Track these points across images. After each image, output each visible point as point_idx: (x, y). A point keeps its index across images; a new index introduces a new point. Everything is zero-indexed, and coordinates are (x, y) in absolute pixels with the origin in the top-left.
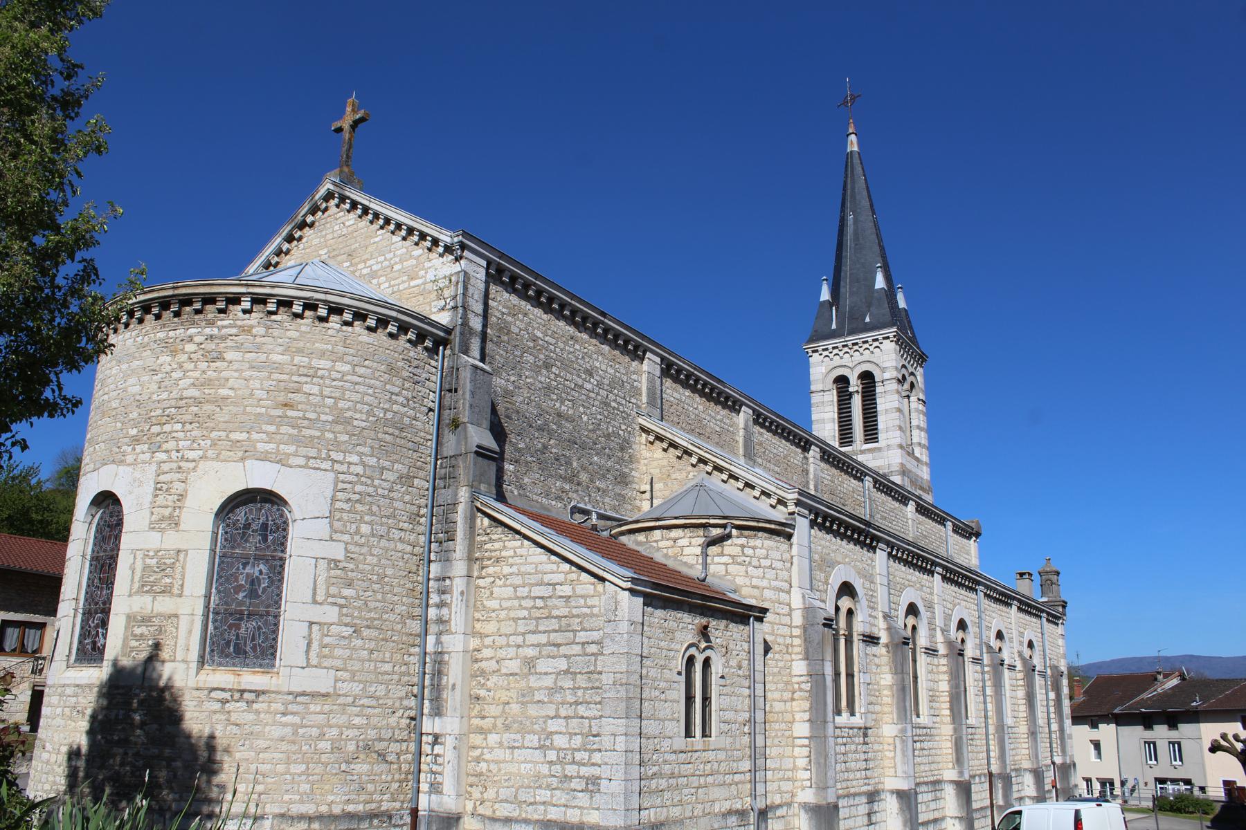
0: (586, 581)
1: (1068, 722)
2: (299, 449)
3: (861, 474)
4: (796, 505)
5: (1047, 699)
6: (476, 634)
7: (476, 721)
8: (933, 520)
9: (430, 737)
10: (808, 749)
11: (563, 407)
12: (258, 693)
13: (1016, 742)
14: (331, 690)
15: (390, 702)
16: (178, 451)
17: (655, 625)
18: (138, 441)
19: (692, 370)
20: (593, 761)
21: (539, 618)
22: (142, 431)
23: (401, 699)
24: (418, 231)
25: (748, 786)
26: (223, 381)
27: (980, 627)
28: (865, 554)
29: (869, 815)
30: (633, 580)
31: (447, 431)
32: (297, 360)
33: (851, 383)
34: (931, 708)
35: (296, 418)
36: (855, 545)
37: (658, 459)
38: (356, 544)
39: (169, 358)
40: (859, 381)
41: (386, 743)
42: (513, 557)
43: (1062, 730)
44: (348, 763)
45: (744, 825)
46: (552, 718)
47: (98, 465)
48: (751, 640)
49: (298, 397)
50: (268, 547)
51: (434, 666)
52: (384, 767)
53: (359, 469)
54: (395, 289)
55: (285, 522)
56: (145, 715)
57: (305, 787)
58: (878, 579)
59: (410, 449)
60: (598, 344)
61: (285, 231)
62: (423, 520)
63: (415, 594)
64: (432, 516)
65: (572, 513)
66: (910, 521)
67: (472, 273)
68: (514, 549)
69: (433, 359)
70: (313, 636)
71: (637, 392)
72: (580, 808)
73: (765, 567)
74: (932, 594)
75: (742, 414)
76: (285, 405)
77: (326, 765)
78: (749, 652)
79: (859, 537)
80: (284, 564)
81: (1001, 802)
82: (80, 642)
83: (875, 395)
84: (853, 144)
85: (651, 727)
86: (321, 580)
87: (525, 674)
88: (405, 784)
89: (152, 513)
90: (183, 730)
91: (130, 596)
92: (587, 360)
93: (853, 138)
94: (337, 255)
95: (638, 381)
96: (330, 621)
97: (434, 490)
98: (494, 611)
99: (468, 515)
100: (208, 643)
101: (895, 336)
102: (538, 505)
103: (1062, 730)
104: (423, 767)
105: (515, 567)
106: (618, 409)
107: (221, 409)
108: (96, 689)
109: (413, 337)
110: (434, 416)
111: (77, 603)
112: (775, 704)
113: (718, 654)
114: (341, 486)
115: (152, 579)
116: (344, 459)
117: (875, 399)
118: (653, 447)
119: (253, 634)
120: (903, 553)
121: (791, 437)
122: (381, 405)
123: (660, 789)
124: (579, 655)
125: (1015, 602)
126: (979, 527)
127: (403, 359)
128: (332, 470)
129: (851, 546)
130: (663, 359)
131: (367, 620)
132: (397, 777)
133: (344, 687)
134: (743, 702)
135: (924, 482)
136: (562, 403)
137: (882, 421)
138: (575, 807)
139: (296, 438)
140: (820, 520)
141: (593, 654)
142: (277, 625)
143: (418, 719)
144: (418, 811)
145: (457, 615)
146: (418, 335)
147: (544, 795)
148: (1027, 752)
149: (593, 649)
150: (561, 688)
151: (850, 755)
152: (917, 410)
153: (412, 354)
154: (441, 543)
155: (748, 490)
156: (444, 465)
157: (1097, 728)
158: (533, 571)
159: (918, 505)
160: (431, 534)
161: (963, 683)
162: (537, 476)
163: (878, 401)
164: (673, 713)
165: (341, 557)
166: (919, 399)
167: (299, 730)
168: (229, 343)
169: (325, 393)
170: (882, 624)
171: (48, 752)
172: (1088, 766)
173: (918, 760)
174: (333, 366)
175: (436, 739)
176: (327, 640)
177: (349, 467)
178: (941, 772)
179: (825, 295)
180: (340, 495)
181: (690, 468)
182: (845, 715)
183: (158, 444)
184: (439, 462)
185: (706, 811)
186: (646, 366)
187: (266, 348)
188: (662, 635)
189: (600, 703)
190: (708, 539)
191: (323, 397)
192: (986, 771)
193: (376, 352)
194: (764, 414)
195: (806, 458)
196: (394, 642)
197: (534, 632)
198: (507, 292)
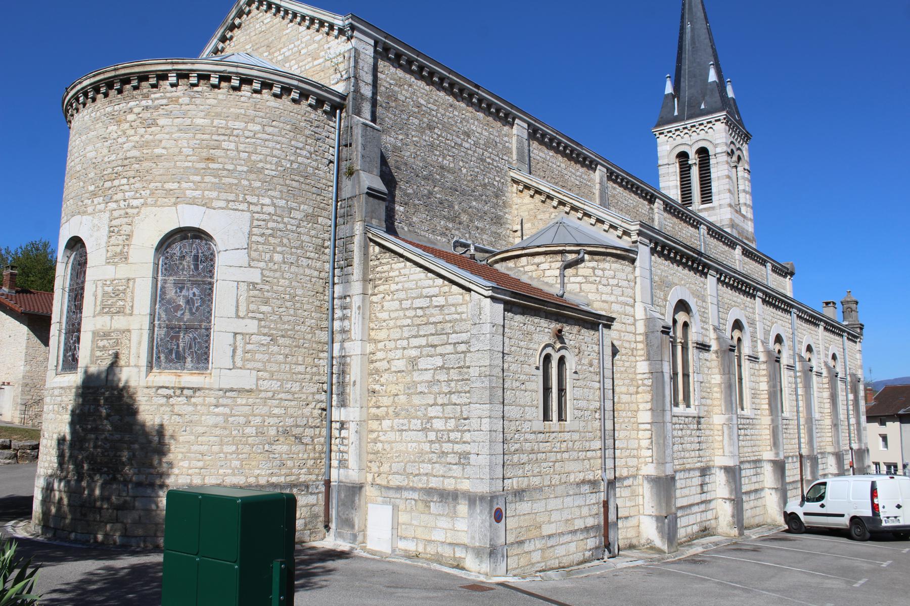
1: (863, 418)
3: (697, 223)
4: (638, 235)
7: (373, 410)
8: (756, 261)
9: (338, 424)
11: (445, 162)
12: (195, 390)
13: (821, 432)
14: (254, 387)
16: (125, 200)
17: (515, 327)
18: (95, 195)
19: (555, 135)
21: (419, 325)
22: (98, 187)
23: (313, 394)
25: (599, 461)
26: (157, 142)
28: (696, 278)
29: (702, 485)
30: (493, 289)
31: (344, 178)
32: (216, 122)
33: (690, 157)
34: (753, 403)
36: (690, 271)
37: (526, 204)
38: (271, 270)
40: (697, 156)
41: (302, 429)
42: (398, 276)
43: (858, 423)
45: (596, 492)
46: (431, 406)
47: (69, 217)
48: (600, 343)
49: (218, 153)
51: (339, 368)
52: (301, 447)
53: (271, 210)
55: (212, 254)
56: (109, 408)
57: (236, 463)
58: (709, 299)
59: (313, 193)
60: (474, 111)
62: (327, 251)
64: (335, 247)
65: (455, 247)
66: (737, 262)
67: (361, 50)
68: (399, 269)
69: (331, 120)
70: (238, 344)
71: (508, 151)
72: (454, 478)
74: (754, 313)
75: (597, 171)
76: (208, 159)
77: (252, 446)
78: (599, 353)
79: (693, 264)
80: (213, 287)
81: (809, 477)
82: (65, 356)
83: (709, 166)
85: (511, 411)
86: (242, 299)
87: (410, 371)
88: (319, 461)
89: (108, 251)
91: (94, 316)
92: (465, 124)
96: (251, 331)
97: (336, 226)
98: (384, 321)
99: (362, 244)
101: (724, 119)
102: (425, 240)
103: (858, 423)
104: (334, 447)
107: (157, 165)
108: (74, 390)
109: (314, 102)
110: (334, 167)
111: (61, 326)
112: (623, 396)
113: (572, 354)
114: (256, 223)
115: (109, 302)
116: (258, 201)
117: (709, 169)
118: (522, 195)
119: (190, 344)
120: (730, 279)
121: (639, 192)
122: (288, 157)
123: (522, 462)
124: (452, 354)
125: (822, 323)
126: (793, 268)
127: (305, 120)
128: (248, 211)
129: (686, 271)
130: (529, 125)
131: (282, 331)
132: (312, 455)
133: (265, 385)
134: (594, 393)
135: (749, 234)
136: (444, 158)
137: (715, 186)
138: (450, 477)
139: (218, 185)
140: (659, 248)
141: (463, 352)
142: (208, 336)
143: (328, 410)
145: (356, 327)
146: (318, 101)
147: (426, 468)
148: (830, 439)
149: (462, 347)
150: (438, 381)
151: (686, 438)
152: (743, 178)
153: (313, 116)
154: (342, 268)
155: (599, 225)
156: (343, 206)
157: (885, 425)
158: (414, 287)
159: (744, 249)
160: (334, 262)
161: (779, 384)
162: (424, 216)
163: (712, 170)
164: (533, 401)
165: (259, 281)
166: (745, 169)
167: (229, 419)
168: (161, 112)
169: (240, 148)
170: (712, 335)
172: (878, 453)
173: (741, 443)
175: (343, 425)
176: (249, 347)
177: (262, 208)
178: (761, 453)
179: (669, 89)
180: (255, 231)
181: (552, 210)
182: (682, 406)
183: (110, 196)
184: (339, 204)
185: (563, 481)
186: (515, 130)
187: (190, 114)
188: (521, 336)
189: (469, 392)
190: (565, 263)
191: (238, 151)
192: (798, 454)
193: (282, 114)
195: (652, 209)
196: (305, 348)
197: (416, 337)
198: (394, 66)
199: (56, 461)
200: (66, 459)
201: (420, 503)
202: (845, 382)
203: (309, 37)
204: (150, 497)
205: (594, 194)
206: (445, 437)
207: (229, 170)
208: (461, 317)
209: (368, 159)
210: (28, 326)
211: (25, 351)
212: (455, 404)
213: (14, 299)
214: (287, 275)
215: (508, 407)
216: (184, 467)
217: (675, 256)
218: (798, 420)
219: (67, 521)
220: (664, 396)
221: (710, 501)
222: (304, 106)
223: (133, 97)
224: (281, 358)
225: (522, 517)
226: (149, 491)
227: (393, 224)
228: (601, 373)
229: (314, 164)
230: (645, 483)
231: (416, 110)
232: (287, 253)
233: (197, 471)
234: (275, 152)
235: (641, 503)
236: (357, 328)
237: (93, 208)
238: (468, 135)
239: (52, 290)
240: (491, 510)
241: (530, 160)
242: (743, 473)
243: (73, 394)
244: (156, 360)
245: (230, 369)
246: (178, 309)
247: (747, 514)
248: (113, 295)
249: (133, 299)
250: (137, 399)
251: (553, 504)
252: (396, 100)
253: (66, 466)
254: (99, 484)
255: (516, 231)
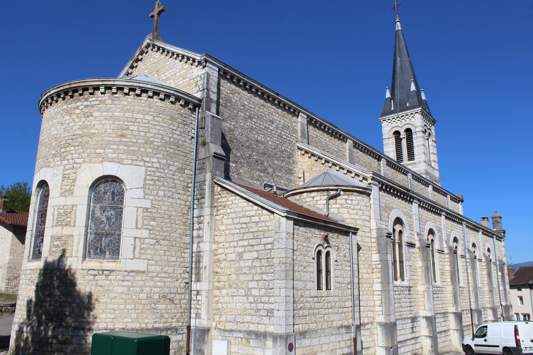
0: (265, 214)
1: (508, 287)
2: (128, 156)
3: (406, 172)
4: (372, 179)
5: (497, 276)
6: (215, 242)
7: (216, 284)
8: (441, 194)
9: (195, 292)
10: (381, 296)
11: (259, 137)
12: (111, 271)
14: (146, 270)
15: (175, 275)
16: (72, 159)
20: (270, 301)
22: (57, 151)
23: (181, 274)
24: (186, 56)
25: (351, 314)
27: (464, 241)
29: (412, 328)
30: (287, 212)
31: (200, 147)
32: (127, 115)
33: (401, 134)
34: (442, 278)
35: (126, 142)
36: (402, 200)
38: (157, 200)
39: (69, 117)
40: (405, 133)
43: (505, 289)
44: (155, 304)
45: (349, 333)
46: (251, 281)
47: (40, 169)
48: (350, 243)
49: (127, 132)
50: (115, 203)
51: (196, 258)
52: (173, 306)
53: (158, 165)
54: (177, 84)
55: (122, 191)
57: (134, 316)
58: (414, 217)
60: (276, 108)
61: (129, 64)
62: (190, 189)
63: (187, 224)
64: (194, 187)
65: (265, 187)
66: (430, 194)
67: (211, 73)
68: (232, 200)
69: (193, 114)
70: (137, 244)
71: (296, 131)
72: (264, 324)
73: (357, 209)
74: (440, 225)
75: (347, 143)
76: (121, 136)
77: (144, 305)
78: (350, 249)
79: (404, 197)
80: (123, 210)
81: (477, 323)
82: (34, 250)
83: (412, 139)
84: (398, 26)
85: (299, 284)
86: (140, 218)
88: (184, 314)
89: (62, 189)
90: (76, 289)
91: (52, 227)
92: (270, 116)
93: (398, 23)
94: (152, 72)
95: (296, 126)
96: (145, 237)
99: (211, 186)
100: (87, 248)
101: (420, 112)
102: (247, 183)
103: (505, 289)
104: (193, 306)
105: (232, 209)
106: (286, 139)
107: (92, 139)
108: (38, 271)
109: (183, 103)
110: (194, 141)
112: (364, 275)
114: (148, 173)
115: (61, 219)
116: (150, 160)
117: (412, 141)
118: (304, 157)
120: (426, 205)
122: (168, 135)
123: (305, 315)
124: (263, 250)
128: (144, 166)
129: (400, 200)
130: (308, 116)
131: (163, 236)
132: (179, 311)
133: (152, 268)
135: (437, 178)
136: (258, 135)
137: (416, 151)
138: (262, 324)
140: (384, 187)
141: (269, 249)
142: (119, 239)
143: (189, 283)
144: (190, 327)
145: (206, 234)
147: (248, 318)
148: (488, 299)
149: (269, 246)
151: (402, 300)
152: (432, 145)
153: (182, 111)
154: (199, 200)
155: (349, 174)
156: (200, 163)
157: (521, 290)
158: (241, 211)
161: (456, 266)
162: (247, 169)
163: (414, 141)
164: (311, 278)
165: (150, 207)
166: (433, 141)
167: (131, 289)
168: (95, 108)
170: (416, 238)
171: (20, 300)
172: (517, 307)
173: (435, 302)
174: (144, 117)
176: (143, 246)
177: (152, 164)
178: (447, 308)
179: (388, 95)
180: (148, 177)
181: (322, 165)
182: (399, 281)
183: (64, 157)
184: (197, 162)
185: (329, 326)
186: (299, 119)
187: (112, 110)
188: (304, 240)
189: (273, 273)
190: (329, 196)
191: (139, 131)
192: (469, 308)
194: (358, 143)
196: (176, 247)
197: (241, 240)
198: (229, 83)
199: (26, 314)
200: (32, 313)
201: (244, 340)
202: (496, 265)
203: (181, 66)
204: (82, 336)
205: (346, 156)
206: (259, 300)
207: (133, 142)
208: (268, 228)
209: (214, 136)
210: (13, 232)
211: (10, 247)
212: (265, 280)
213: (5, 216)
214: (166, 204)
215: (296, 282)
216: (103, 318)
217: (394, 192)
218: (469, 288)
219: (31, 351)
220: (388, 275)
221: (418, 337)
222: (178, 106)
223: (79, 100)
224: (162, 252)
225: (305, 348)
226: (81, 332)
227: (228, 174)
228: (351, 261)
229: (183, 139)
230: (379, 326)
231: (242, 108)
232: (167, 191)
233: (111, 320)
234: (161, 132)
235: (376, 339)
236: (207, 235)
237: (54, 163)
238: (272, 122)
239: (28, 211)
240: (286, 343)
241: (308, 136)
242: (437, 320)
243: (38, 273)
244: (88, 253)
245: (132, 259)
246: (102, 223)
247: (440, 346)
248: (64, 215)
249: (75, 217)
250: (76, 276)
251: (323, 340)
252: (231, 102)
253: (31, 317)
254: (51, 328)
255: (300, 178)
